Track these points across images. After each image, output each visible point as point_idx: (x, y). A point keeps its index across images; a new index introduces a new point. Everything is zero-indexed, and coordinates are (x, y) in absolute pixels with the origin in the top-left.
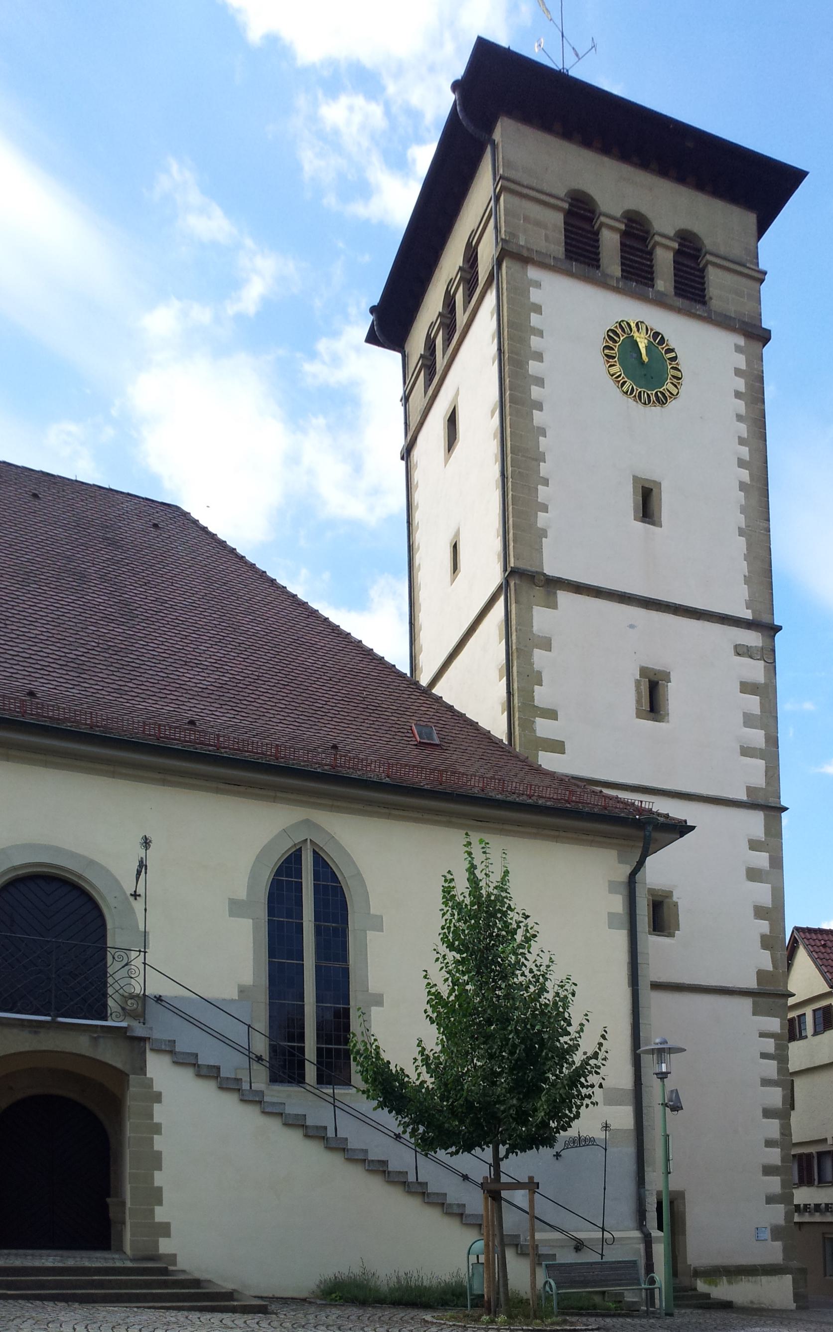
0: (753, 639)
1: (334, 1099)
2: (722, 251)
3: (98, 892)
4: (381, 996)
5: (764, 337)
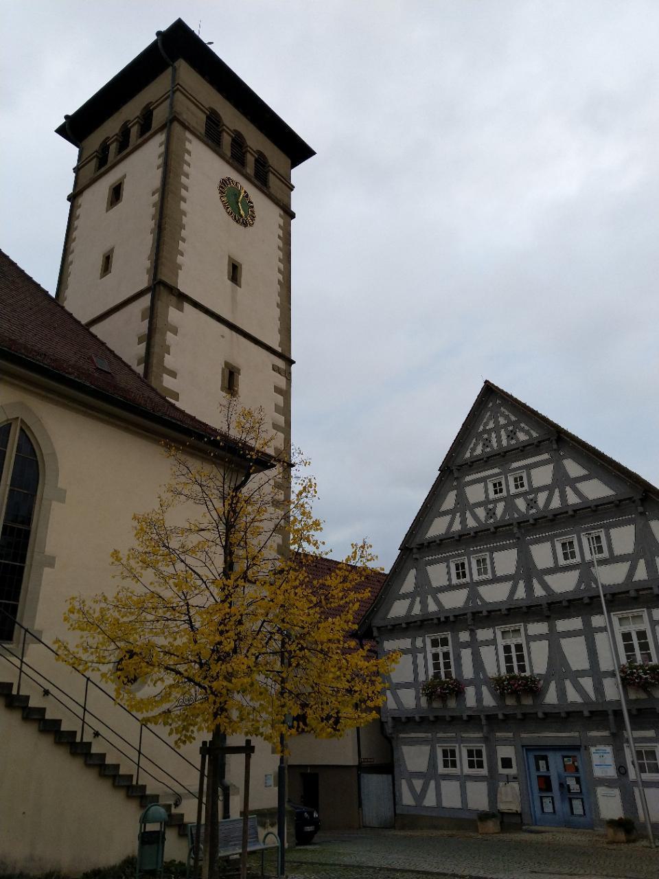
0: (281, 363)
1: (20, 669)
2: (276, 168)
3: (44, 479)
4: (54, 558)
5: (292, 216)
